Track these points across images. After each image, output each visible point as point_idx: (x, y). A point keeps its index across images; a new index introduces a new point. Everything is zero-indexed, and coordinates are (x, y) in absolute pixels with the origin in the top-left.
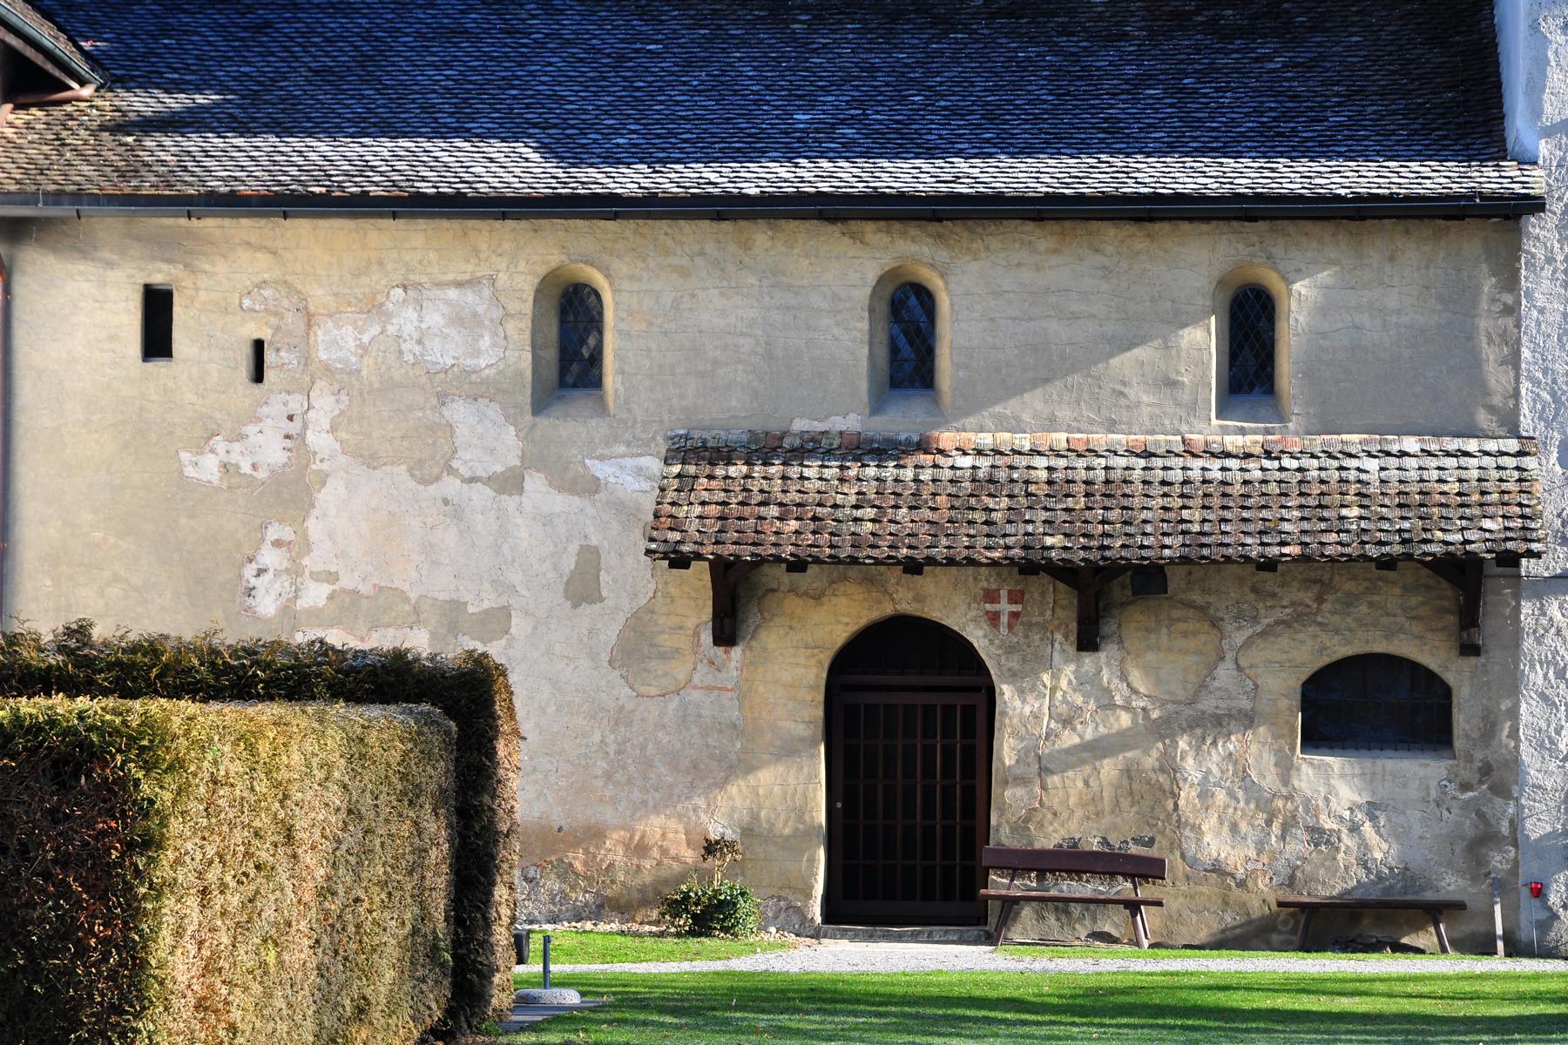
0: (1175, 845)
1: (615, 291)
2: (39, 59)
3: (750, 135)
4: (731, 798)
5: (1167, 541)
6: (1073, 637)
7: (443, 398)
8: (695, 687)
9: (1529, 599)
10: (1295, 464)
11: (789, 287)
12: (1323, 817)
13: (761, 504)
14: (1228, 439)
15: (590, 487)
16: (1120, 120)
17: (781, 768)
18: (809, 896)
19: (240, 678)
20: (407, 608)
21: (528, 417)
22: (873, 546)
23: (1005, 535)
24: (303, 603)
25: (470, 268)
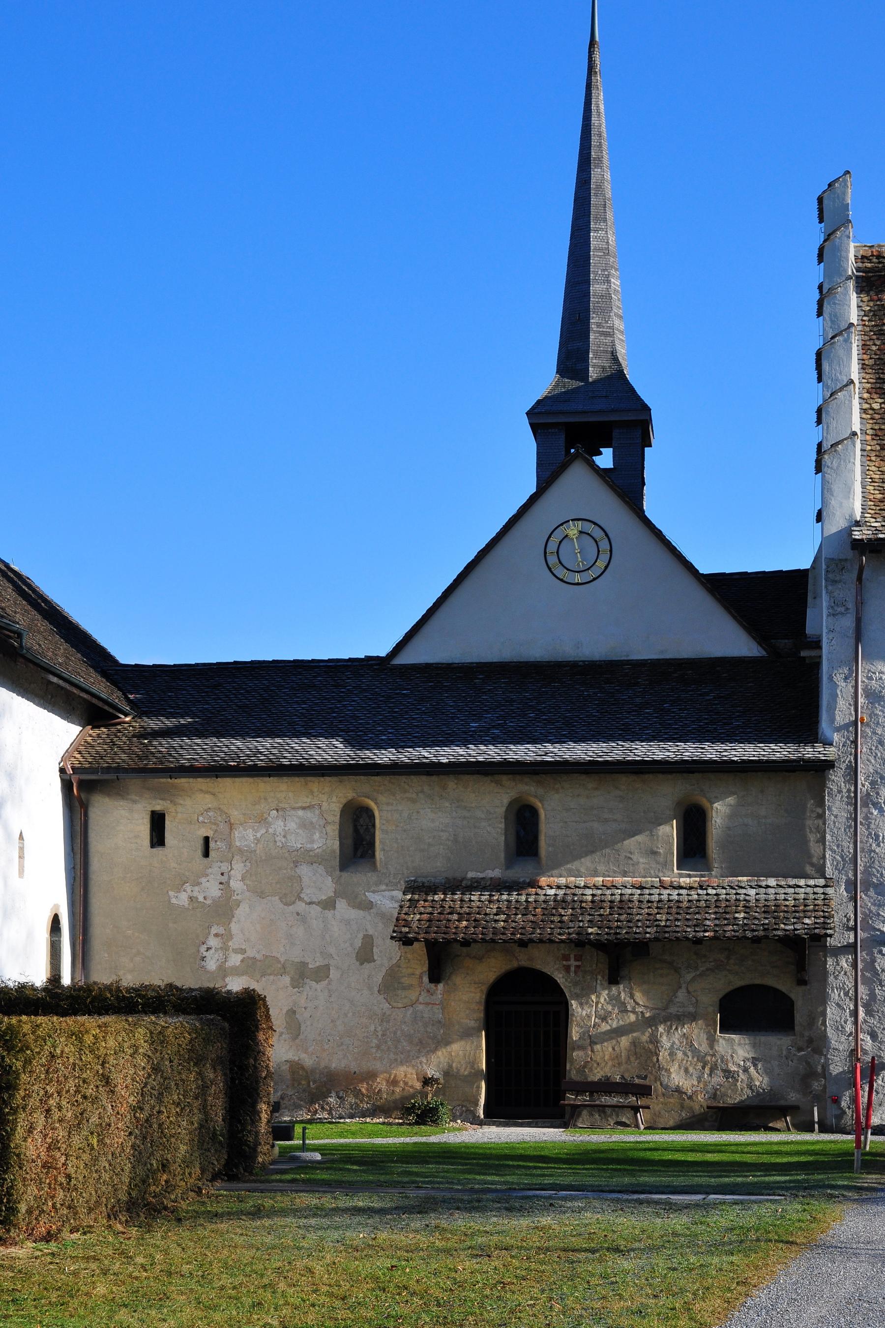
0: (657, 1079)
1: (380, 811)
2: (100, 704)
3: (447, 734)
4: (438, 1057)
5: (648, 930)
6: (606, 978)
7: (296, 863)
8: (420, 1003)
9: (831, 956)
10: (714, 892)
11: (465, 808)
12: (730, 1065)
13: (449, 914)
14: (682, 880)
15: (368, 906)
16: (631, 725)
17: (463, 1043)
18: (476, 1104)
19: (130, 1003)
20: (279, 966)
21: (338, 872)
22: (503, 934)
23: (569, 928)
24: (229, 964)
25: (309, 800)
